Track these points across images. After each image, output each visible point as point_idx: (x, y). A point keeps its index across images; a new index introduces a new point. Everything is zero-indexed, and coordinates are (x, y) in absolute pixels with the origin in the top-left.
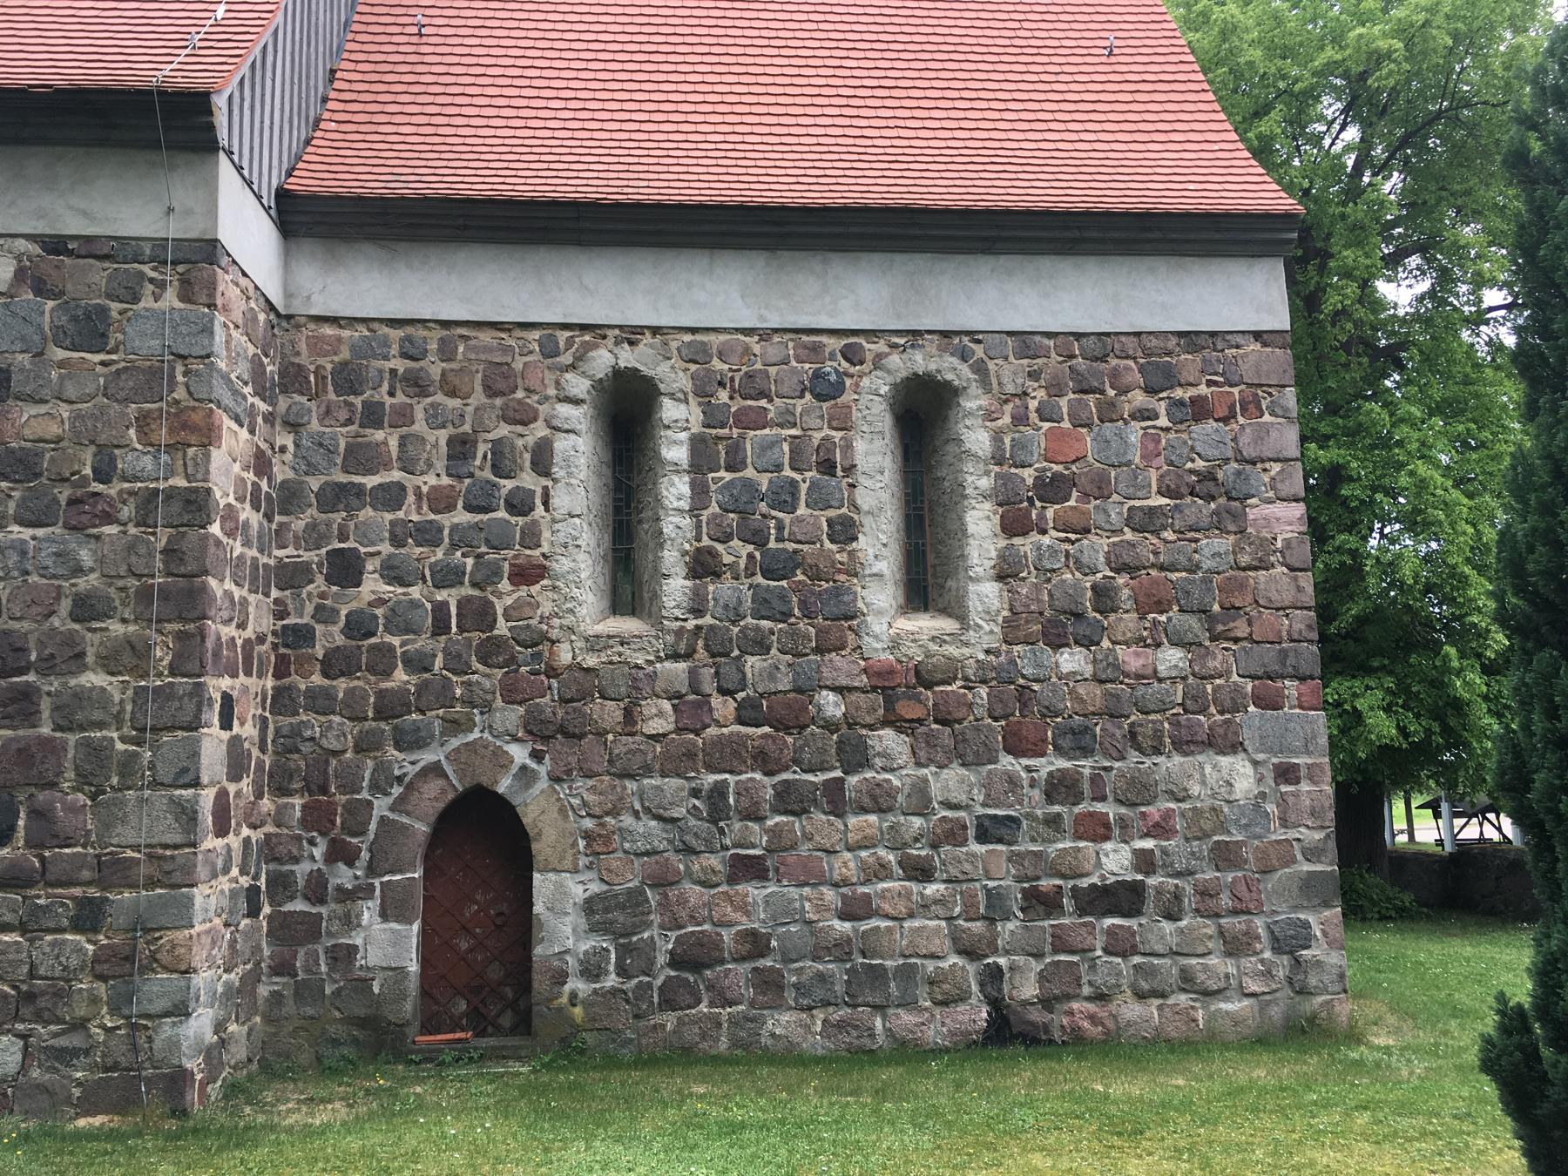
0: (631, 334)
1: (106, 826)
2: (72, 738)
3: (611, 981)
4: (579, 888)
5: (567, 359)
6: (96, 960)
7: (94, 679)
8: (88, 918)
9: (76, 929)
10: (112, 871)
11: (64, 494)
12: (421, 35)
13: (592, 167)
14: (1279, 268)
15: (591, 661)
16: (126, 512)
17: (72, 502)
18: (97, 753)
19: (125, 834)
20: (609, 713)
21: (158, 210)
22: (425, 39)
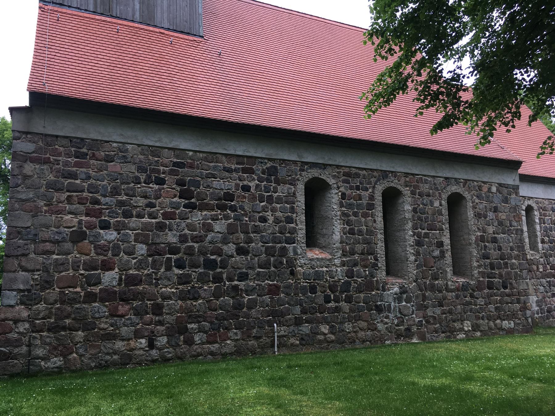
0: (530, 198)
1: (519, 286)
2: (513, 271)
3: (540, 315)
4: (535, 299)
5: (522, 202)
6: (520, 308)
7: (514, 261)
8: (518, 302)
9: (517, 303)
10: (519, 293)
11: (507, 229)
12: (58, 20)
13: (70, 83)
14: (28, 105)
15: (532, 258)
16: (514, 232)
17: (508, 230)
18: (516, 273)
19: (521, 287)
20: (535, 267)
21: (512, 180)
22: (59, 22)
